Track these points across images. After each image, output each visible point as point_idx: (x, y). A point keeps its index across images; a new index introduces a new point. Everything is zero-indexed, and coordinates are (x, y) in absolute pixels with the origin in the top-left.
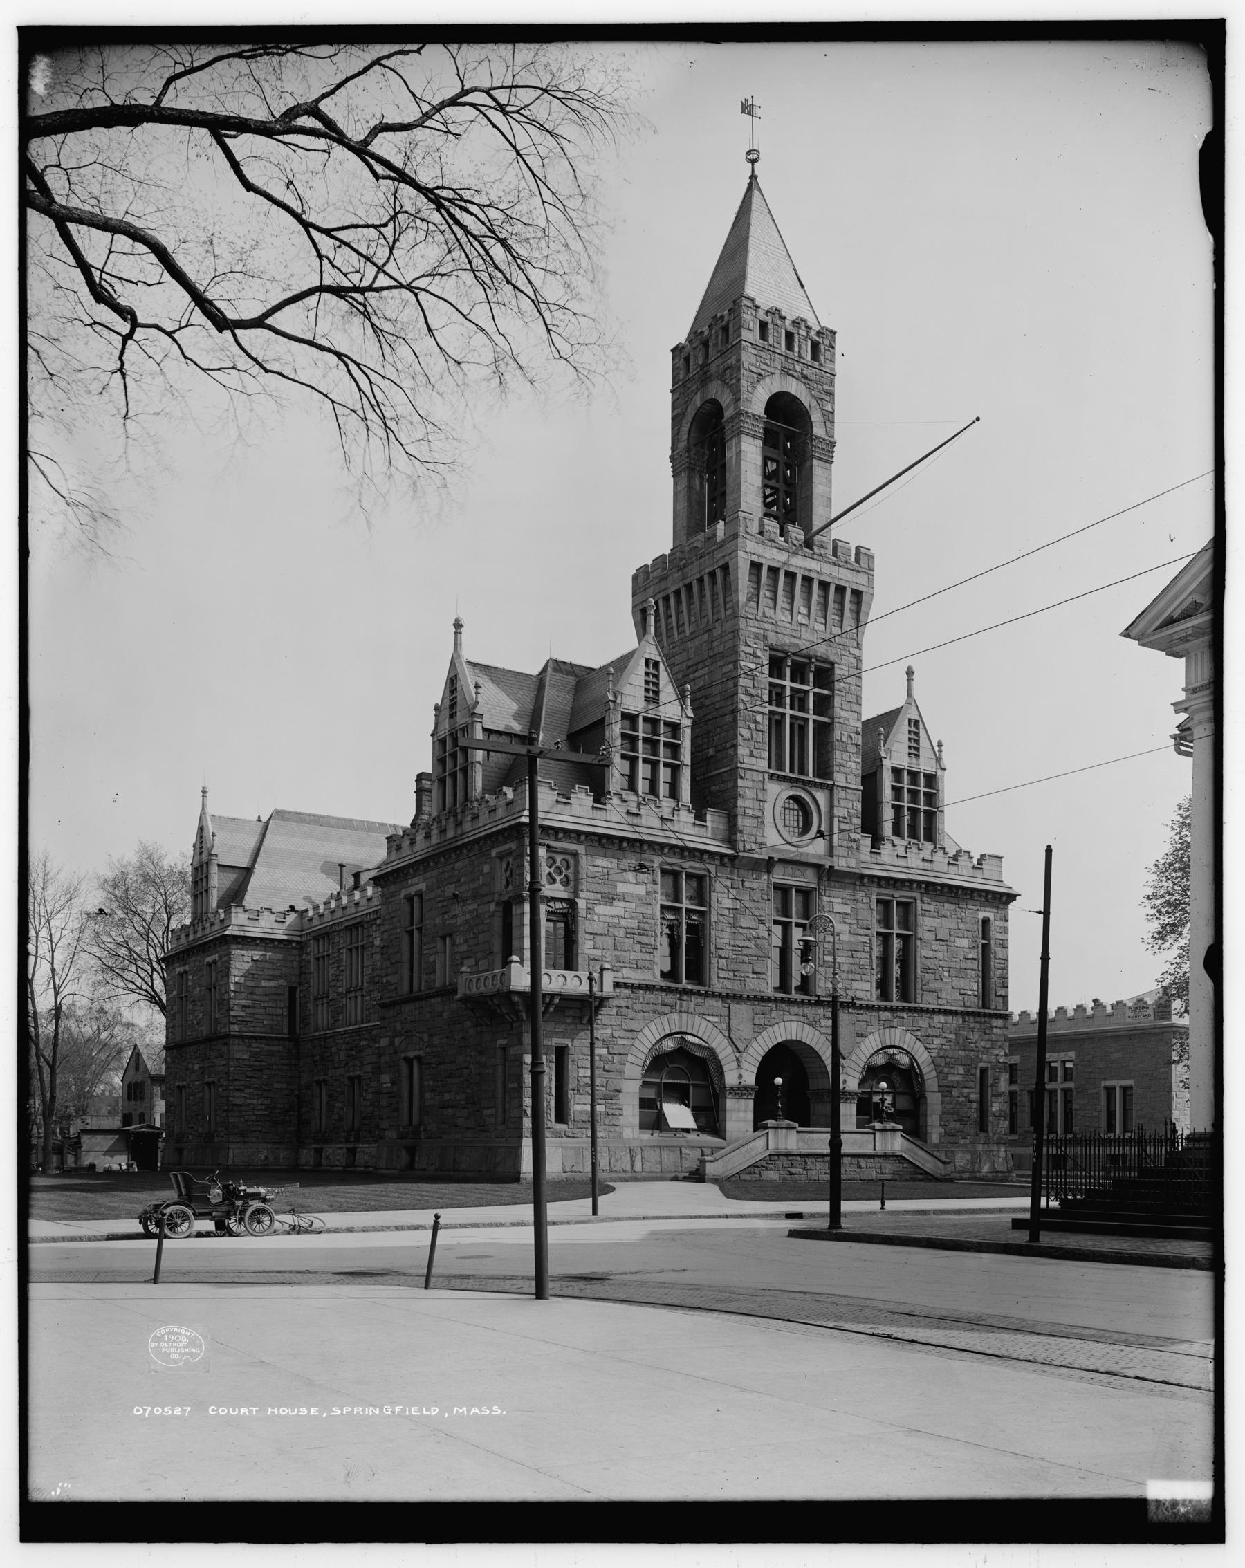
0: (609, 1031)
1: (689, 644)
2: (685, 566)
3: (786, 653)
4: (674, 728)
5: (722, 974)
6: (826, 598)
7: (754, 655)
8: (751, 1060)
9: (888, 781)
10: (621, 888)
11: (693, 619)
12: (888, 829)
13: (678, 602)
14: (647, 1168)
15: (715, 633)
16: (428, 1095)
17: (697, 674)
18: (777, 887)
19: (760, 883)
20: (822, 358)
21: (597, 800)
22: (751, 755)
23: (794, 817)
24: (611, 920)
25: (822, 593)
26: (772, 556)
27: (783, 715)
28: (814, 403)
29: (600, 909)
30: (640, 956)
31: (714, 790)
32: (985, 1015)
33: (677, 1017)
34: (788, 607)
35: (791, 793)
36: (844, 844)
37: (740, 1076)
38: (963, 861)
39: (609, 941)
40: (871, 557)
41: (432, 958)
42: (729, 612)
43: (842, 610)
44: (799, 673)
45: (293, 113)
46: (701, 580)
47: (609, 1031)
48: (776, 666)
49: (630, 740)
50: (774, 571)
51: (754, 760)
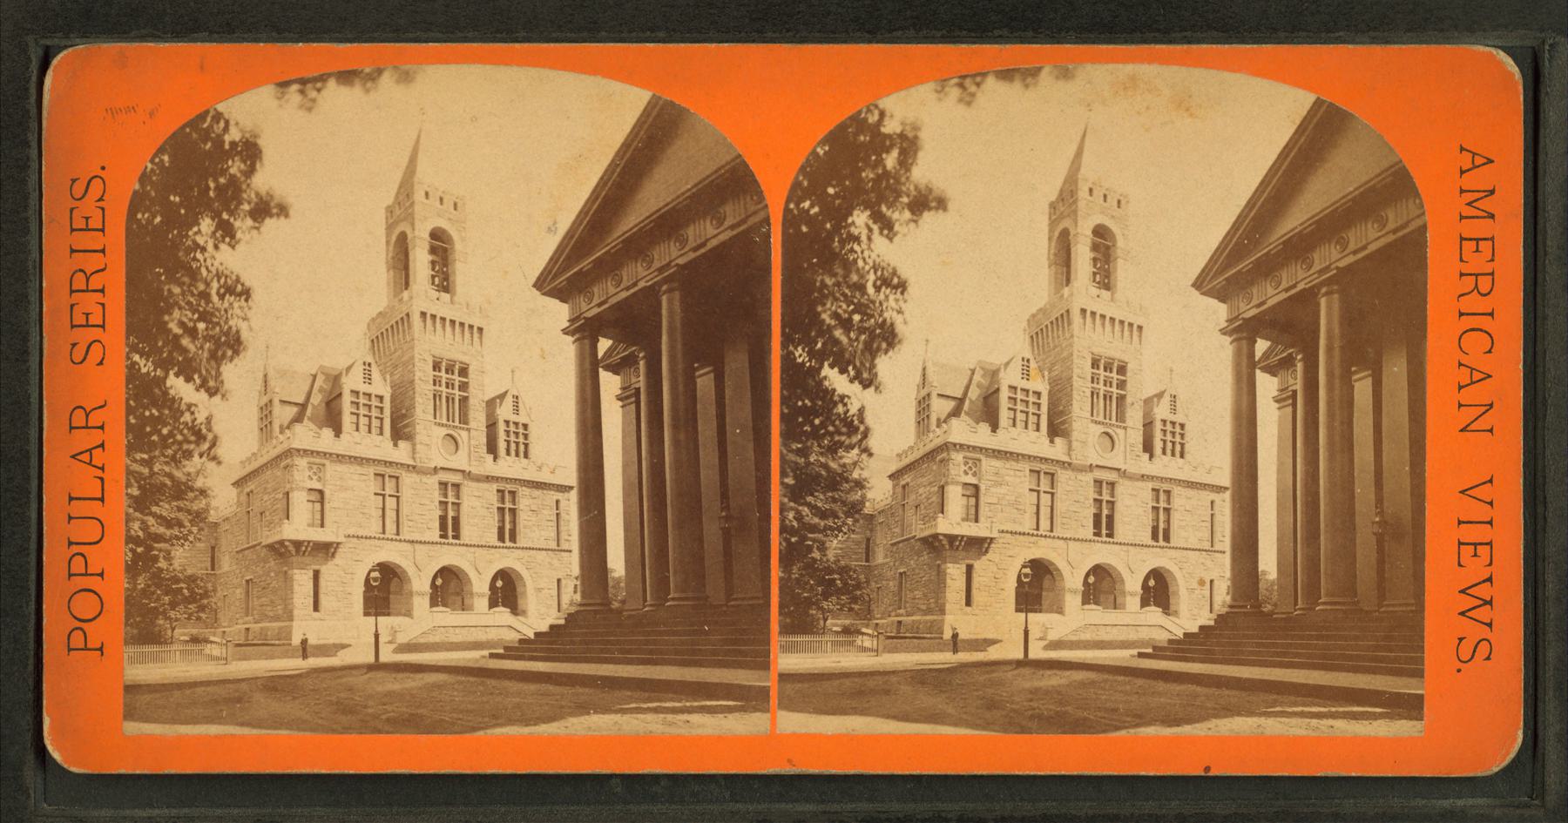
9: (501, 427)
19: (1088, 478)
21: (994, 431)
31: (401, 430)
38: (545, 469)
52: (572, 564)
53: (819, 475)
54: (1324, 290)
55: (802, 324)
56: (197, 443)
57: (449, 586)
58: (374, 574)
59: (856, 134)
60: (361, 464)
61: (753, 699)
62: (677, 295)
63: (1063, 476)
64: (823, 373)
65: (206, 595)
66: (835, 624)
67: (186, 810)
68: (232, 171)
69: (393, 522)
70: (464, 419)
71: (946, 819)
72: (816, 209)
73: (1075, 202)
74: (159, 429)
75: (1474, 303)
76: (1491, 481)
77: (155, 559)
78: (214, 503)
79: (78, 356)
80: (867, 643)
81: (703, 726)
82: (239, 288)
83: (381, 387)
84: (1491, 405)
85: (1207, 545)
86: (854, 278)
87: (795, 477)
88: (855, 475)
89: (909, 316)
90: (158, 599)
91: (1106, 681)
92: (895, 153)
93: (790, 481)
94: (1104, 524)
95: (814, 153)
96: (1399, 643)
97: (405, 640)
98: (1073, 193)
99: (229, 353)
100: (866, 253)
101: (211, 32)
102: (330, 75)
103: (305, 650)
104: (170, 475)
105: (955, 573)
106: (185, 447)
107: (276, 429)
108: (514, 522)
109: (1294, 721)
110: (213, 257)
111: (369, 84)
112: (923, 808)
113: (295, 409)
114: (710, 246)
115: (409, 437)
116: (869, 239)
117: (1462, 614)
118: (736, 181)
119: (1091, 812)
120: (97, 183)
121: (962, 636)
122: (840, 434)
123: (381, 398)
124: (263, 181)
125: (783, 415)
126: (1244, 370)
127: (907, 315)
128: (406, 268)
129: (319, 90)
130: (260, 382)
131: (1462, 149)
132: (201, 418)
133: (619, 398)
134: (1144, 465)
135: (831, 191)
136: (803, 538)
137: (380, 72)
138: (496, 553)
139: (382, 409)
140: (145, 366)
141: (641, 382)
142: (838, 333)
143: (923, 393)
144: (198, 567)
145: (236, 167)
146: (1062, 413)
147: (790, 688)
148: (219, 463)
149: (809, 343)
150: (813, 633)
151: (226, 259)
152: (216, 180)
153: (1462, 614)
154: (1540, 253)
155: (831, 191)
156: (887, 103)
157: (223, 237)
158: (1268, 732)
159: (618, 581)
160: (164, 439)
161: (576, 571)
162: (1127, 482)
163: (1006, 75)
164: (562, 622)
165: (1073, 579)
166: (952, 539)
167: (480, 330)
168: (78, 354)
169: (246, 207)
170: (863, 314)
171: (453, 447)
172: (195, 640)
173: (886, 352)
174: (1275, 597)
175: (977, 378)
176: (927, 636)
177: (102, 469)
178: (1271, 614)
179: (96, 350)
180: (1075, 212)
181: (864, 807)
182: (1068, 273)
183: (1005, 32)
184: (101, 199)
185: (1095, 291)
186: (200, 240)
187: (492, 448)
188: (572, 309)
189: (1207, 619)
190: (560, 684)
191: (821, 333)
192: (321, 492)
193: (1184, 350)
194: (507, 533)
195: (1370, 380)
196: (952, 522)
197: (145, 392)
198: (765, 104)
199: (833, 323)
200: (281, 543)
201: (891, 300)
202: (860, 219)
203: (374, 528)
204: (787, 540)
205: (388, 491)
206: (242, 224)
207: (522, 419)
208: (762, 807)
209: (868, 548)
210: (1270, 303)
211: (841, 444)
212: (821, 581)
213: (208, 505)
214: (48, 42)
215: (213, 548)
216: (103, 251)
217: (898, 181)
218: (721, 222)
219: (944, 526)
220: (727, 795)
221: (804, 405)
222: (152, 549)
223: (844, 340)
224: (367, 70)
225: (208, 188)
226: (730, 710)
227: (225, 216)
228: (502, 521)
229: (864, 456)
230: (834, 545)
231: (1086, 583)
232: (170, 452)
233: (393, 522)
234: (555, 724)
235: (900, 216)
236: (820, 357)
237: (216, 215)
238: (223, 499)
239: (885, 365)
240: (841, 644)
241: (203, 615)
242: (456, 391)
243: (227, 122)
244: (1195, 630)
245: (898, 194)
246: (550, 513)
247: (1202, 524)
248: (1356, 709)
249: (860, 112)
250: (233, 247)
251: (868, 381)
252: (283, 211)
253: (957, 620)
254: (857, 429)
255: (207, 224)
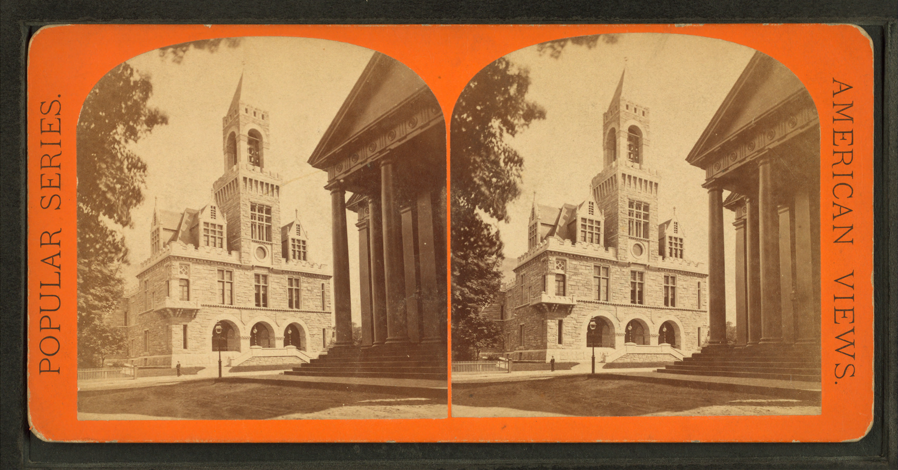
4: (598, 223)
9: (667, 240)
12: (291, 256)
18: (632, 272)
21: (196, 248)
26: (628, 172)
29: (574, 277)
49: (584, 226)
52: (331, 320)
53: (474, 270)
54: (761, 161)
55: (464, 183)
56: (116, 254)
57: (261, 334)
58: (593, 323)
59: (493, 75)
60: (210, 265)
61: (438, 397)
62: (390, 166)
63: (614, 269)
64: (475, 212)
65: (121, 340)
66: (484, 355)
67: (111, 464)
68: (135, 98)
69: (229, 298)
70: (269, 238)
71: (546, 468)
72: (470, 118)
73: (238, 116)
74: (99, 247)
75: (841, 169)
76: (852, 274)
77: (93, 319)
78: (126, 287)
79: (45, 204)
80: (128, 372)
81: (407, 412)
82: (140, 164)
83: (221, 221)
84: (852, 227)
85: (696, 308)
86: (493, 157)
87: (460, 271)
88: (495, 270)
89: (526, 178)
90: (470, 335)
91: (640, 386)
92: (515, 86)
93: (457, 273)
94: (637, 296)
95: (469, 86)
96: (801, 364)
97: (236, 365)
98: (236, 111)
99: (134, 201)
100: (499, 143)
101: (124, 18)
102: (190, 43)
103: (179, 370)
104: (100, 272)
105: (552, 325)
106: (109, 255)
107: (161, 243)
108: (673, 295)
109: (747, 407)
110: (124, 147)
111: (213, 48)
112: (532, 462)
113: (172, 233)
114: (409, 138)
115: (238, 249)
116: (501, 135)
117: (837, 350)
118: (424, 102)
119: (628, 464)
120: (56, 104)
121: (556, 361)
122: (486, 246)
123: (221, 227)
124: (152, 104)
125: (452, 236)
126: (716, 208)
127: (523, 179)
128: (615, 149)
129: (184, 51)
130: (530, 212)
131: (834, 81)
132: (118, 238)
133: (734, 224)
134: (660, 263)
135: (479, 108)
136: (465, 306)
137: (219, 41)
138: (632, 310)
139: (599, 229)
140: (86, 210)
141: (370, 216)
142: (483, 189)
143: (533, 222)
144: (118, 324)
145: (137, 95)
146: (612, 233)
147: (460, 392)
148: (129, 264)
149: (466, 194)
150: (471, 360)
151: (132, 148)
152: (126, 104)
153: (837, 350)
154: (886, 143)
155: (479, 108)
156: (133, 62)
157: (130, 136)
158: (733, 413)
159: (358, 330)
160: (97, 251)
161: (334, 324)
162: (273, 275)
163: (577, 41)
164: (326, 353)
165: (245, 331)
166: (550, 305)
167: (656, 184)
168: (45, 203)
169: (143, 118)
170: (497, 177)
171: (262, 254)
172: (115, 365)
173: (135, 205)
174: (735, 337)
175: (186, 217)
176: (539, 361)
177: (59, 267)
178: (733, 346)
179: (56, 200)
180: (619, 118)
181: (499, 461)
182: (615, 154)
183: (579, 18)
184: (58, 114)
185: (251, 167)
186: (117, 138)
187: (285, 255)
188: (708, 174)
189: (696, 350)
190: (324, 389)
191: (473, 189)
192: (187, 281)
193: (682, 198)
194: (294, 302)
195: (788, 213)
196: (550, 296)
197: (88, 224)
198: (438, 59)
199: (481, 183)
200: (165, 309)
201: (138, 175)
202: (495, 124)
203: (218, 301)
204: (456, 308)
205: (226, 280)
206: (141, 128)
207: (302, 238)
208: (440, 461)
209: (502, 311)
210: (731, 169)
211: (486, 252)
212: (100, 337)
213: (122, 288)
214: (31, 24)
215: (502, 307)
216: (59, 144)
217: (517, 103)
218: (414, 124)
219: (169, 303)
220: (421, 454)
221: (465, 230)
222: (91, 313)
223: (487, 192)
224: (212, 40)
225: (121, 108)
226: (422, 403)
227: (131, 123)
228: (667, 294)
229: (499, 259)
230: (106, 316)
231: (252, 333)
232: (100, 258)
233: (229, 298)
234: (323, 412)
235: (518, 122)
236: (474, 203)
237: (126, 123)
238: (131, 285)
239: (511, 208)
240: (488, 366)
241: (495, 345)
242: (642, 219)
243: (132, 70)
244: (690, 356)
245: (140, 115)
246: (317, 291)
247: (693, 295)
248: (782, 400)
249: (495, 62)
250: (513, 136)
251: (501, 216)
252: (542, 115)
253: (554, 353)
254: (120, 250)
255: (120, 129)
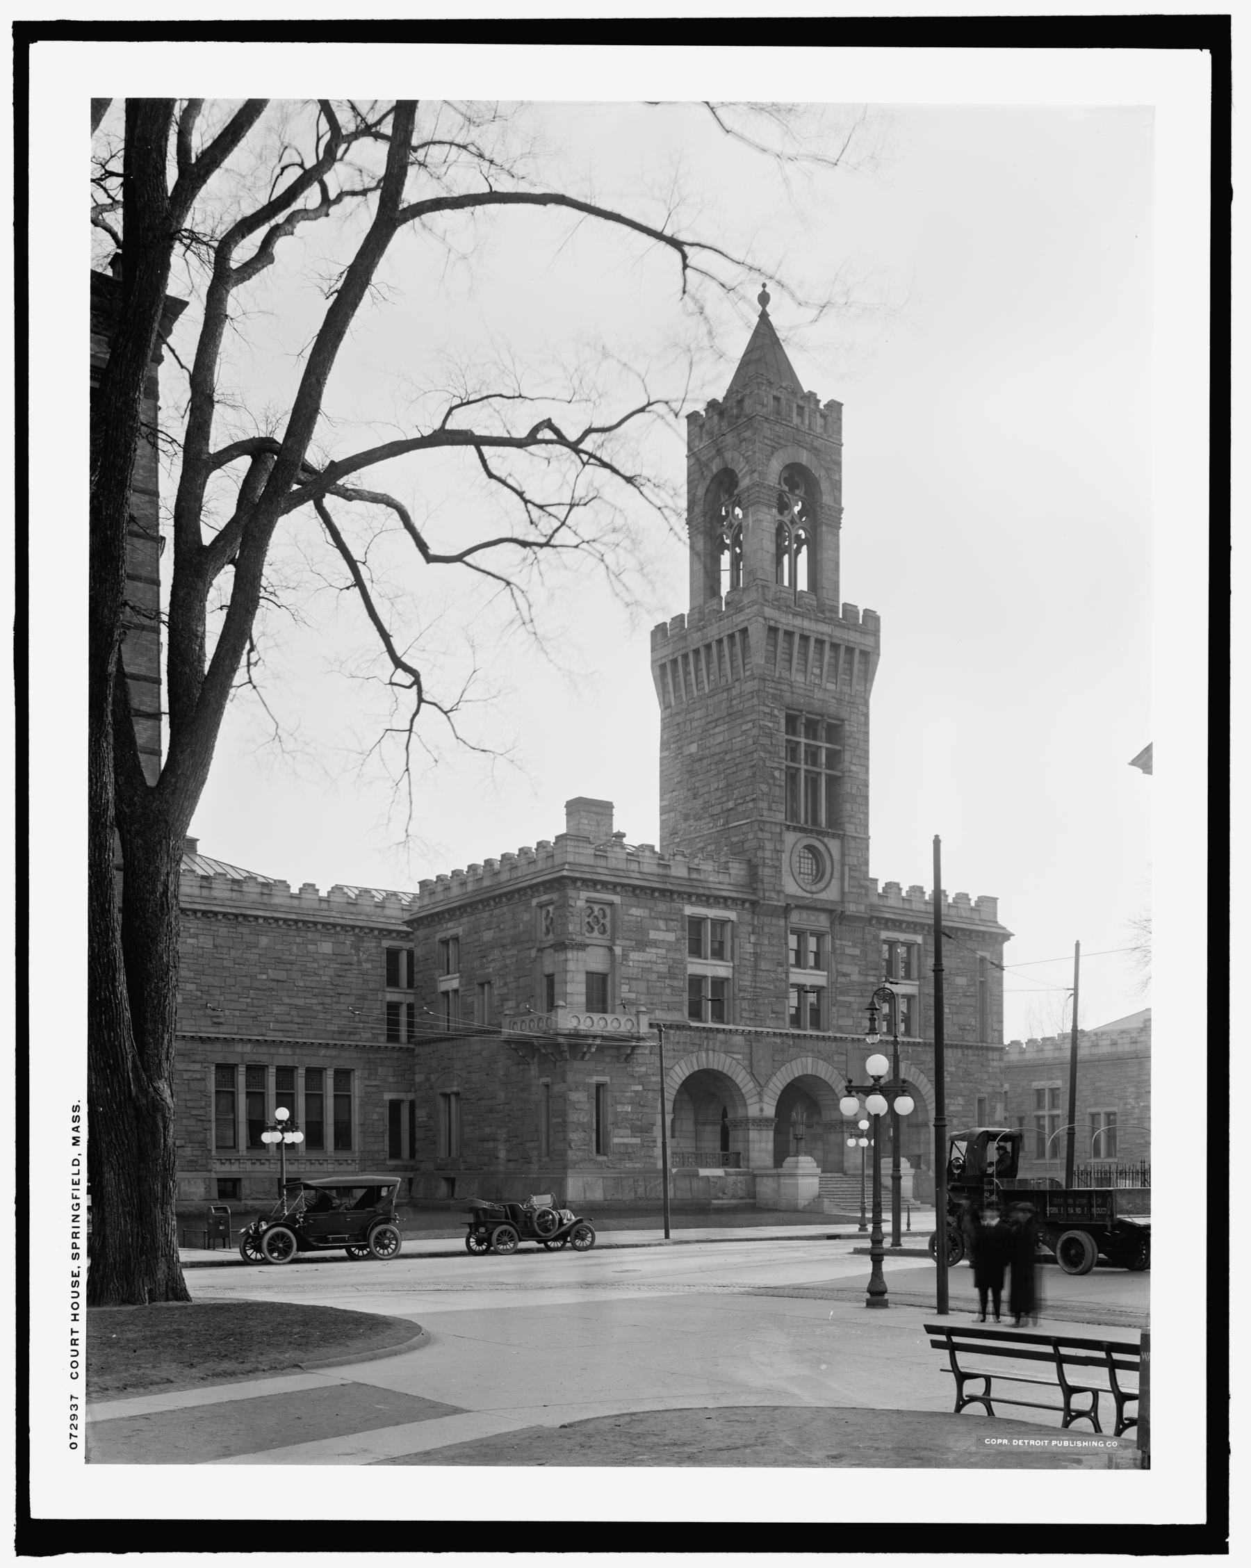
0: (643, 1069)
1: (709, 701)
2: (704, 627)
3: (801, 711)
5: (745, 1014)
6: (837, 658)
7: (772, 715)
8: (771, 1094)
10: (653, 935)
11: (712, 678)
13: (697, 660)
14: (679, 1196)
15: (735, 692)
16: (468, 1129)
17: (717, 730)
20: (830, 432)
22: (770, 809)
23: (808, 865)
24: (645, 966)
25: (833, 654)
27: (798, 769)
28: (823, 473)
29: (634, 956)
30: (671, 999)
32: (982, 1048)
33: (704, 1055)
34: (803, 668)
35: (806, 842)
36: (854, 890)
37: (761, 1110)
39: (642, 986)
40: (877, 619)
41: (470, 999)
42: (748, 673)
43: (851, 670)
44: (812, 728)
45: (536, 429)
46: (720, 641)
47: (643, 1069)
48: (791, 721)
50: (789, 634)
51: (772, 814)
